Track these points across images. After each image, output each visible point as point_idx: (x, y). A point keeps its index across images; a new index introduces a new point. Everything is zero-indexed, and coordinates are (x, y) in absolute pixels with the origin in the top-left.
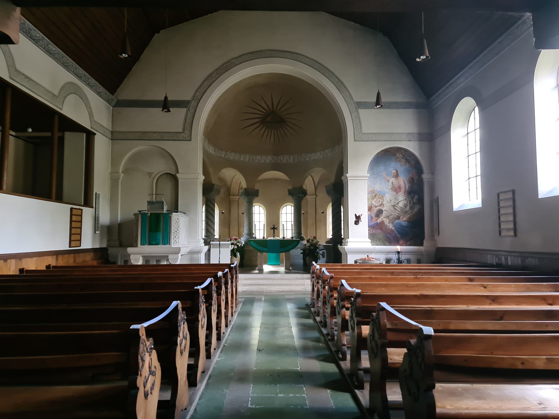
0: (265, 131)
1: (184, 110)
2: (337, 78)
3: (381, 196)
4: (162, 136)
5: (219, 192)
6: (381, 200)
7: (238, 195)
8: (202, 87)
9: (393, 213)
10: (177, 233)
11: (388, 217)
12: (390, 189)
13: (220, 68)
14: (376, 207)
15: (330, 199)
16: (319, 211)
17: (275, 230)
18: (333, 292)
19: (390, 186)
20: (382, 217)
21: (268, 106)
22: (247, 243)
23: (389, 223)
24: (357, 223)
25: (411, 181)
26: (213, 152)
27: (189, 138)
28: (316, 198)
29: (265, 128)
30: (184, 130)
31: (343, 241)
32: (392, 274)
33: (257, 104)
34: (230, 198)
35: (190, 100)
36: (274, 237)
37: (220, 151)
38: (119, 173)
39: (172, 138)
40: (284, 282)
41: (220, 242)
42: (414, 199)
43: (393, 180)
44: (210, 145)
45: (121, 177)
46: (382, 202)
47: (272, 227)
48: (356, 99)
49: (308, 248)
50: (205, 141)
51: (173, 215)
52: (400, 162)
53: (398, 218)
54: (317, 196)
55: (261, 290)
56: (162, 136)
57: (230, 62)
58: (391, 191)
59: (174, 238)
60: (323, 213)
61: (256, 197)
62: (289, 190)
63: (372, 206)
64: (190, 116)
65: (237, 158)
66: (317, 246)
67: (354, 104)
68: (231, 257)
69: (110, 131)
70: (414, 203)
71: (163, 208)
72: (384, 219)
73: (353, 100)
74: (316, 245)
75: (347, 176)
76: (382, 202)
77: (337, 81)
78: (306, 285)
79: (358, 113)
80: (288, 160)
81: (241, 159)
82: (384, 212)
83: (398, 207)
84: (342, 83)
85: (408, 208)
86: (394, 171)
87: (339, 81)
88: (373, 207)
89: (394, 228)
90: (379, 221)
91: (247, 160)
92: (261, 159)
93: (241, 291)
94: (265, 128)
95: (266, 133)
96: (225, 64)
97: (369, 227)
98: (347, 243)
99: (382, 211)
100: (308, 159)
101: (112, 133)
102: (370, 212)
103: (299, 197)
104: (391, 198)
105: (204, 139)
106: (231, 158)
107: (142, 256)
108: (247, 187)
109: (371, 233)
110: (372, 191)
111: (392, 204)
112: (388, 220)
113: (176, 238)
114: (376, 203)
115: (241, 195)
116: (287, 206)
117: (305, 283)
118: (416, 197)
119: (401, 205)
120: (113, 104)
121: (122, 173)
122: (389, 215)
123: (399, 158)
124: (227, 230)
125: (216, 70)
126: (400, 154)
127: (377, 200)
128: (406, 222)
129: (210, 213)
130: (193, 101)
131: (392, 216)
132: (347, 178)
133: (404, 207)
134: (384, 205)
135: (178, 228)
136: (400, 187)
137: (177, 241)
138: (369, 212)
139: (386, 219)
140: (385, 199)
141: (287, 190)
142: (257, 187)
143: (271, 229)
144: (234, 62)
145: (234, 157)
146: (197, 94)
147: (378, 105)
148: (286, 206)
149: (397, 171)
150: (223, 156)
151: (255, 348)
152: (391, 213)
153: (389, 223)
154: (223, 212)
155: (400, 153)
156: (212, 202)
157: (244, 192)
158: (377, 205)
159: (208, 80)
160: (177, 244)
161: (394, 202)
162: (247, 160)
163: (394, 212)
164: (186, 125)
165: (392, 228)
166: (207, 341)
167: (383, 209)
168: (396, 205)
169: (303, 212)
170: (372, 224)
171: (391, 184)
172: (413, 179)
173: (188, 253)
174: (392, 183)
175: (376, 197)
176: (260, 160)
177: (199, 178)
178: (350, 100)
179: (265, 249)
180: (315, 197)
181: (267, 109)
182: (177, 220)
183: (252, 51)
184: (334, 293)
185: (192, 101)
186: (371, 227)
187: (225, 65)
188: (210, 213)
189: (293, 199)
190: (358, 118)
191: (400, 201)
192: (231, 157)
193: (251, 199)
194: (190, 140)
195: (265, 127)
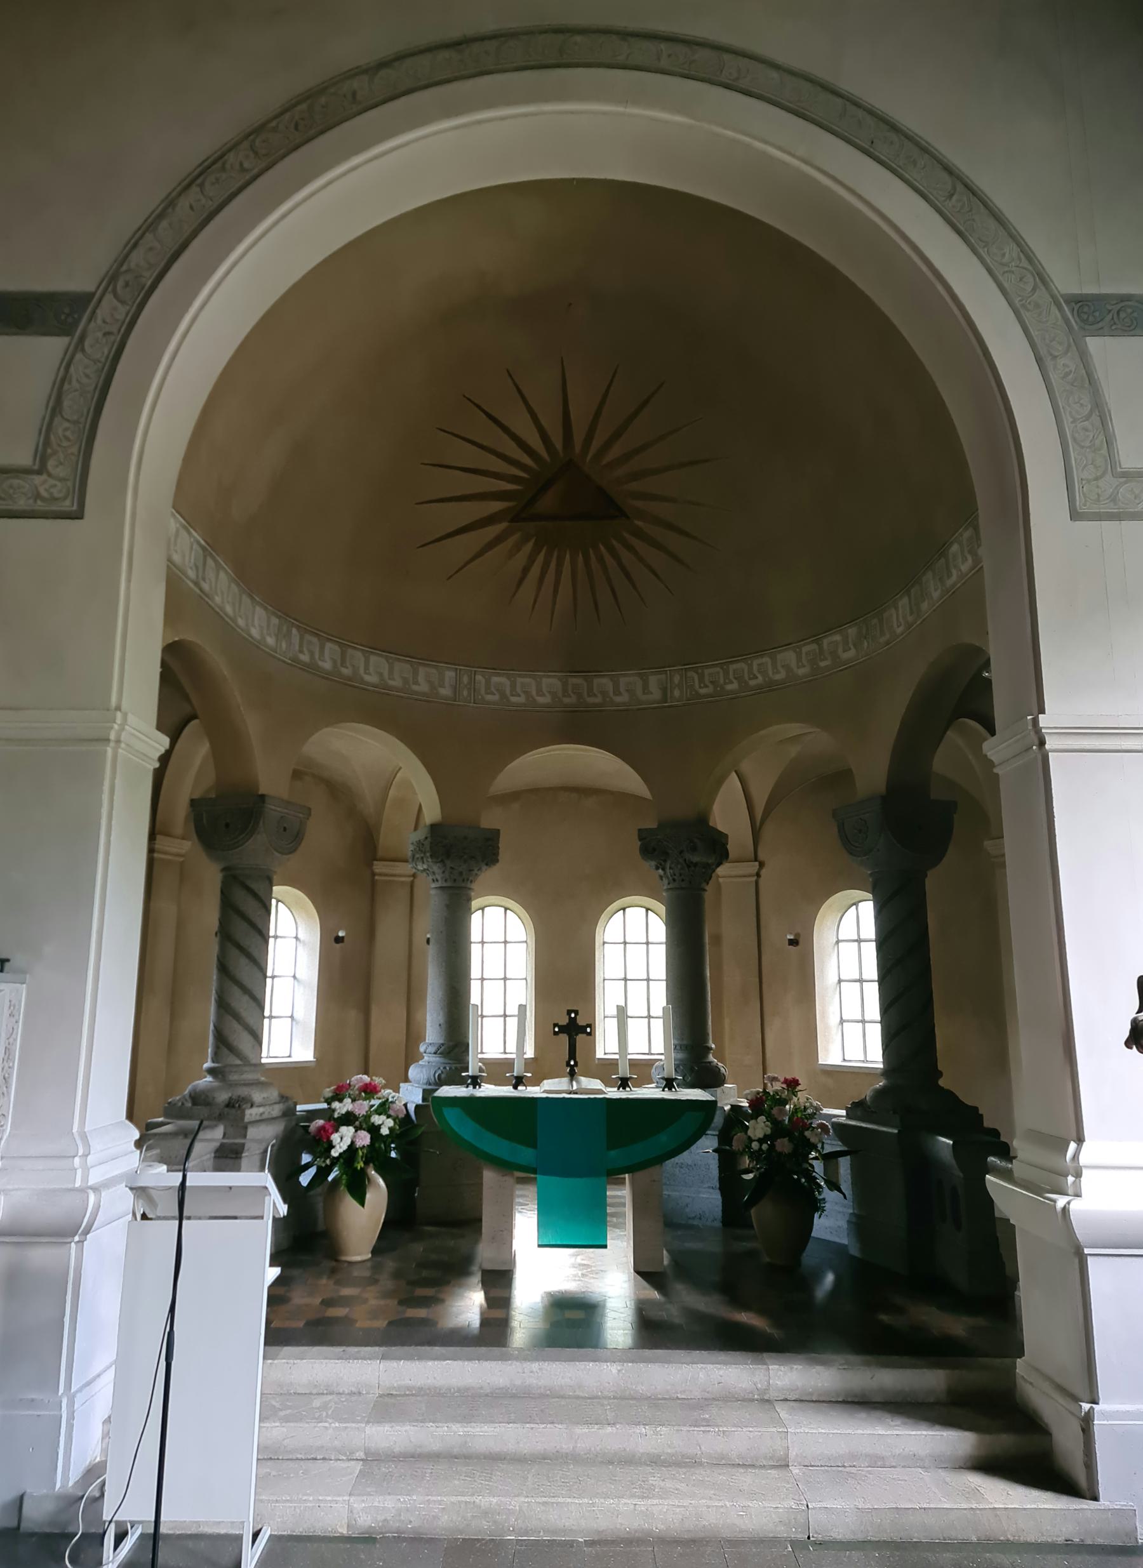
0: (531, 560)
1: (52, 347)
2: (949, 170)
13: (273, 124)
16: (777, 933)
17: (580, 1038)
26: (270, 641)
28: (758, 875)
29: (529, 546)
34: (377, 871)
35: (93, 294)
36: (572, 1075)
37: (308, 637)
41: (184, 1177)
44: (252, 598)
47: (564, 1021)
48: (1066, 283)
49: (765, 1147)
55: (485, 1524)
60: (794, 942)
61: (484, 867)
62: (643, 835)
64: (84, 372)
65: (397, 683)
66: (813, 1140)
67: (1054, 310)
68: (274, 1273)
74: (807, 1134)
79: (1084, 356)
80: (639, 692)
81: (415, 688)
84: (974, 194)
87: (960, 187)
91: (445, 691)
92: (540, 692)
94: (529, 546)
95: (536, 569)
98: (1078, 1175)
103: (696, 865)
105: (204, 549)
106: (367, 678)
108: (443, 818)
115: (413, 856)
116: (627, 910)
117: (792, 1454)
124: (353, 1016)
125: (249, 135)
130: (109, 297)
132: (1042, 743)
141: (636, 833)
142: (489, 820)
143: (556, 1033)
144: (354, 94)
145: (381, 675)
146: (136, 258)
148: (624, 909)
150: (327, 665)
154: (341, 934)
156: (254, 886)
157: (429, 839)
159: (201, 186)
162: (445, 691)
164: (60, 432)
176: (508, 692)
177: (112, 736)
178: (1029, 288)
179: (526, 1155)
181: (544, 453)
183: (455, 34)
187: (304, 106)
189: (661, 877)
192: (369, 674)
193: (461, 873)
194: (78, 515)
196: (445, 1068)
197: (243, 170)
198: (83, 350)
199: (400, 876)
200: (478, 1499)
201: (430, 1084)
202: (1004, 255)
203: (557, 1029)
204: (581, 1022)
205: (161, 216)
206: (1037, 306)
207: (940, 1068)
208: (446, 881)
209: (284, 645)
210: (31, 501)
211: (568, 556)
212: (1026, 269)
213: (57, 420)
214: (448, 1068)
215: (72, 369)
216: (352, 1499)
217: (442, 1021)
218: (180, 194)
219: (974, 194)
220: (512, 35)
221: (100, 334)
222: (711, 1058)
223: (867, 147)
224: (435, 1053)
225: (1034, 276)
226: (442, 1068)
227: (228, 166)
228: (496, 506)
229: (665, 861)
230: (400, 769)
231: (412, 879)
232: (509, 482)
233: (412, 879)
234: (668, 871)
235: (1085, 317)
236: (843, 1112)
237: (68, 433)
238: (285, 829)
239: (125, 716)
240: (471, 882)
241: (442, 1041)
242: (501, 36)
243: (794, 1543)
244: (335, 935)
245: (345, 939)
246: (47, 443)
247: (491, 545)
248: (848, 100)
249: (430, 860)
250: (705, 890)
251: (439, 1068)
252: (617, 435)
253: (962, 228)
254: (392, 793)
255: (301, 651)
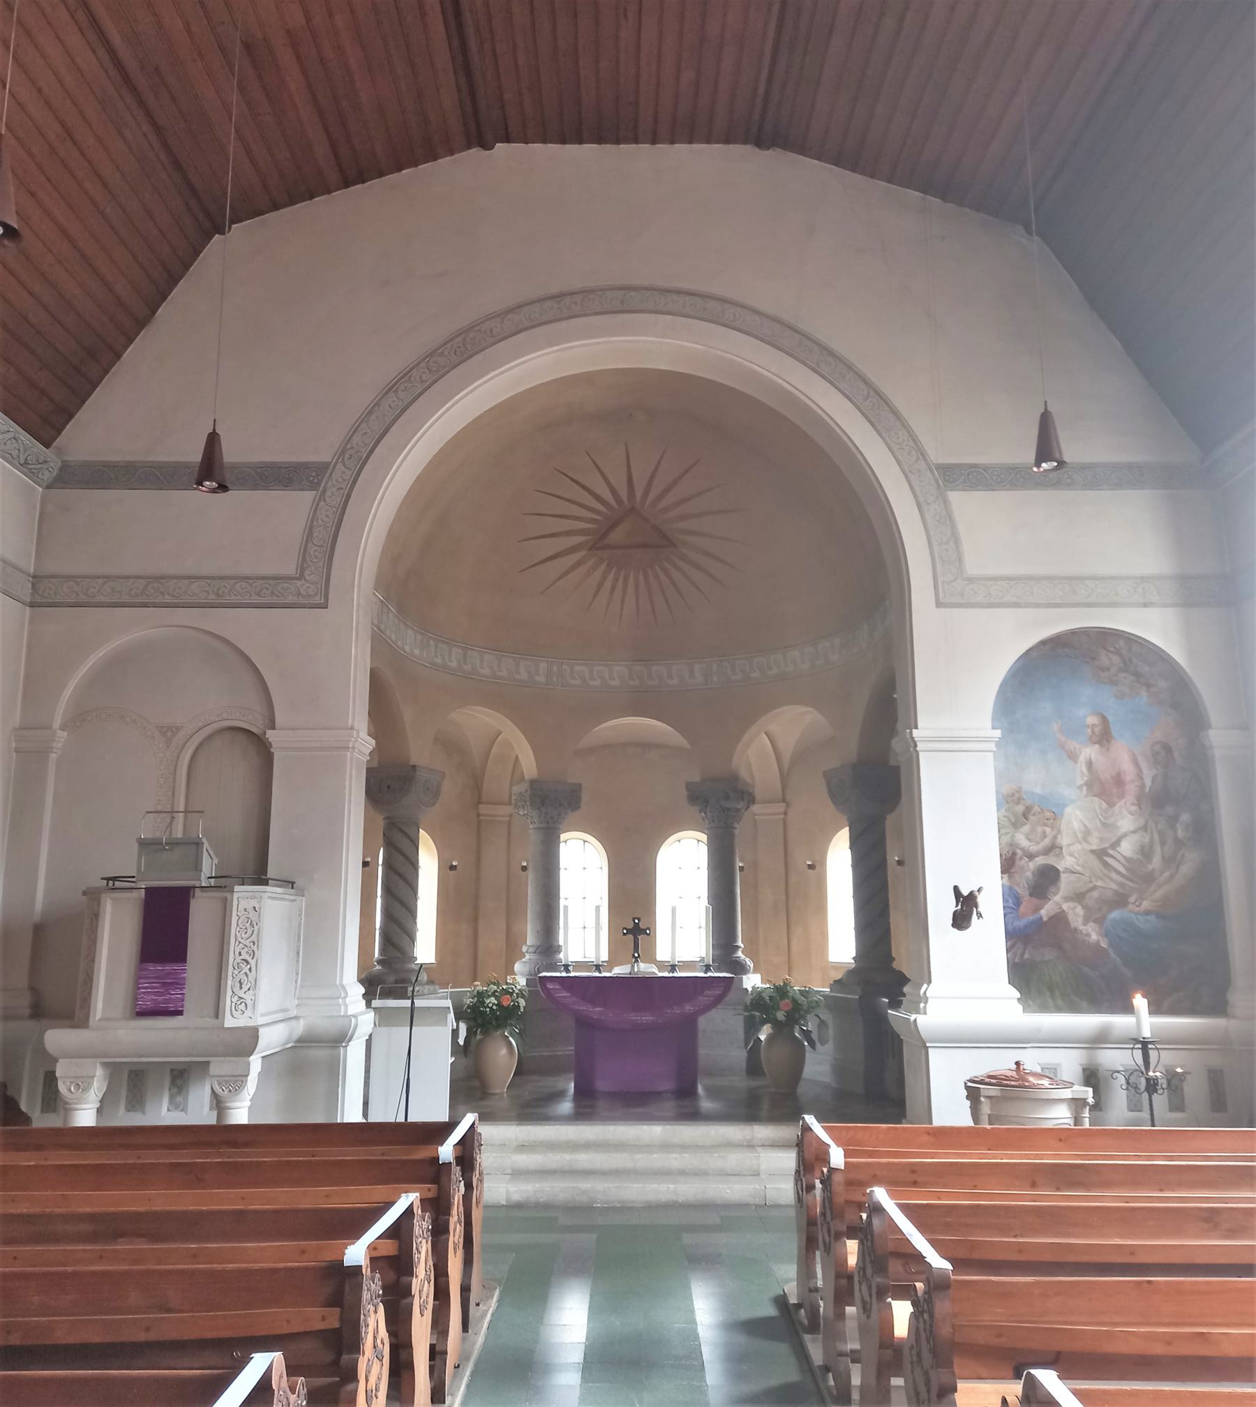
0: (604, 578)
2: (865, 381)
3: (1048, 814)
4: (220, 592)
5: (437, 794)
6: (1048, 830)
7: (510, 804)
8: (373, 417)
9: (1099, 883)
10: (250, 969)
11: (1078, 897)
12: (1080, 788)
14: (1031, 857)
15: (844, 819)
18: (949, 1364)
19: (1080, 773)
20: (1057, 898)
21: (614, 492)
22: (538, 983)
23: (1085, 923)
24: (961, 920)
25: (1163, 754)
27: (318, 596)
28: (785, 813)
29: (603, 567)
30: (302, 567)
31: (906, 989)
32: (1206, 1220)
33: (577, 483)
34: (481, 812)
37: (440, 645)
38: (50, 727)
39: (256, 599)
40: (675, 1161)
42: (1178, 826)
43: (1090, 752)
45: (58, 745)
46: (1055, 837)
47: (631, 925)
48: (937, 455)
50: (385, 609)
51: (236, 896)
52: (1113, 682)
53: (1120, 900)
54: (788, 806)
56: (220, 592)
57: (477, 328)
58: (1086, 796)
59: (237, 989)
60: (811, 867)
61: (570, 812)
62: (690, 787)
63: (1014, 854)
67: (929, 473)
69: (29, 575)
70: (1179, 843)
71: (197, 867)
72: (1065, 906)
73: (925, 460)
75: (913, 738)
76: (1055, 837)
77: (865, 393)
78: (763, 1176)
79: (946, 502)
81: (517, 676)
82: (1062, 876)
83: (1119, 857)
84: (881, 398)
85: (1156, 862)
86: (1092, 720)
87: (872, 394)
88: (1018, 857)
89: (1106, 939)
90: (1045, 913)
91: (541, 678)
93: (504, 1203)
94: (603, 567)
95: (608, 584)
96: (459, 335)
97: (1010, 934)
99: (1057, 872)
100: (756, 675)
101: (36, 579)
102: (1010, 877)
104: (1087, 824)
106: (574, 682)
107: (105, 1065)
109: (1016, 960)
110: (1013, 795)
111: (1094, 847)
112: (1080, 910)
113: (245, 988)
114: (1030, 840)
118: (1185, 817)
119: (1127, 848)
120: (47, 476)
121: (63, 728)
122: (1083, 890)
123: (1108, 669)
126: (1111, 655)
127: (1033, 830)
128: (1152, 918)
129: (401, 876)
130: (340, 465)
131: (1095, 894)
132: (916, 746)
133: (1140, 857)
134: (1061, 848)
135: (255, 948)
136: (1119, 781)
137: (249, 1002)
138: (1006, 876)
139: (1071, 904)
140: (1063, 827)
144: (491, 331)
146: (356, 439)
147: (1046, 462)
149: (1105, 720)
150: (454, 664)
151: (577, 1356)
152: (1090, 882)
153: (1085, 923)
154: (454, 864)
155: (1111, 652)
157: (529, 793)
158: (1034, 848)
160: (248, 1013)
161: (1102, 839)
163: (1102, 880)
164: (312, 553)
165: (1098, 942)
166: (394, 1341)
167: (1059, 868)
168: (1111, 852)
169: (741, 865)
170: (1020, 923)
171: (1084, 769)
172: (1167, 749)
173: (299, 1041)
174: (1090, 764)
175: (1031, 818)
176: (587, 678)
180: (783, 810)
181: (613, 503)
182: (252, 915)
184: (956, 1369)
185: (335, 465)
186: (1015, 937)
187: (459, 339)
188: (401, 876)
189: (703, 819)
190: (948, 522)
191: (1125, 835)
193: (552, 817)
195: (605, 564)
196: (542, 963)
197: (422, 381)
198: (325, 500)
199: (502, 816)
200: (579, 1185)
201: (531, 975)
202: (898, 438)
203: (625, 931)
204: (642, 926)
205: (370, 413)
206: (919, 471)
207: (894, 956)
208: (541, 823)
209: (425, 654)
210: (295, 597)
211: (632, 574)
212: (912, 447)
213: (310, 545)
214: (544, 963)
215: (318, 512)
216: (508, 1186)
217: (539, 929)
218: (382, 398)
219: (881, 398)
220: (592, 291)
221: (335, 489)
222: (740, 954)
223: (814, 366)
224: (535, 953)
225: (916, 451)
226: (540, 963)
227: (412, 379)
228: (579, 539)
229: (706, 807)
230: (501, 733)
231: (508, 818)
232: (587, 522)
233: (508, 818)
234: (708, 814)
235: (947, 478)
236: (829, 990)
237: (317, 553)
238: (428, 789)
239: (358, 731)
240: (560, 824)
241: (539, 944)
242: (584, 292)
243: (757, 1206)
244: (450, 864)
245: (458, 868)
246: (304, 560)
247: (573, 568)
248: (803, 335)
249: (529, 808)
250: (559, 829)
251: (538, 964)
252: (667, 490)
253: (873, 420)
254: (494, 750)
255: (437, 657)
